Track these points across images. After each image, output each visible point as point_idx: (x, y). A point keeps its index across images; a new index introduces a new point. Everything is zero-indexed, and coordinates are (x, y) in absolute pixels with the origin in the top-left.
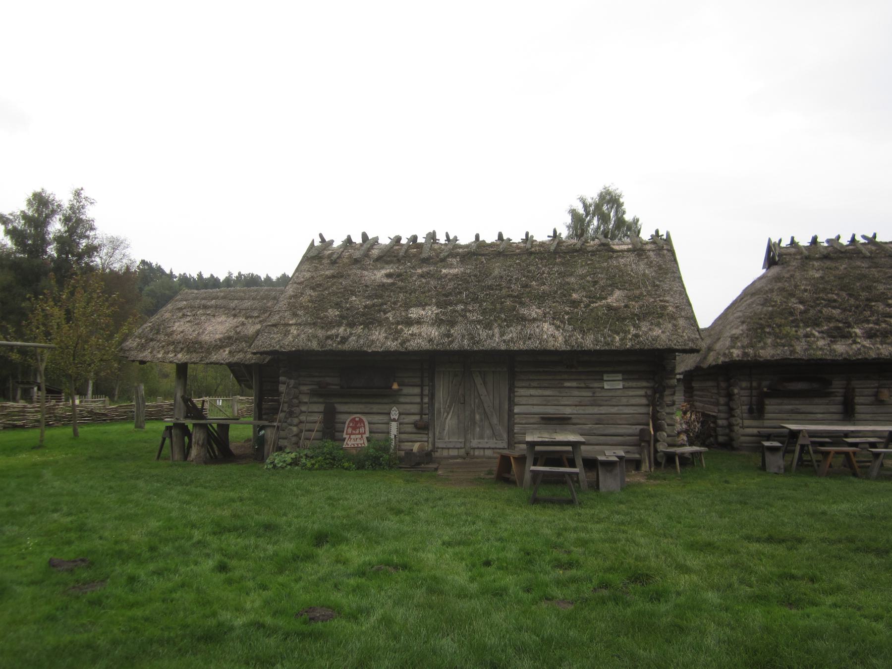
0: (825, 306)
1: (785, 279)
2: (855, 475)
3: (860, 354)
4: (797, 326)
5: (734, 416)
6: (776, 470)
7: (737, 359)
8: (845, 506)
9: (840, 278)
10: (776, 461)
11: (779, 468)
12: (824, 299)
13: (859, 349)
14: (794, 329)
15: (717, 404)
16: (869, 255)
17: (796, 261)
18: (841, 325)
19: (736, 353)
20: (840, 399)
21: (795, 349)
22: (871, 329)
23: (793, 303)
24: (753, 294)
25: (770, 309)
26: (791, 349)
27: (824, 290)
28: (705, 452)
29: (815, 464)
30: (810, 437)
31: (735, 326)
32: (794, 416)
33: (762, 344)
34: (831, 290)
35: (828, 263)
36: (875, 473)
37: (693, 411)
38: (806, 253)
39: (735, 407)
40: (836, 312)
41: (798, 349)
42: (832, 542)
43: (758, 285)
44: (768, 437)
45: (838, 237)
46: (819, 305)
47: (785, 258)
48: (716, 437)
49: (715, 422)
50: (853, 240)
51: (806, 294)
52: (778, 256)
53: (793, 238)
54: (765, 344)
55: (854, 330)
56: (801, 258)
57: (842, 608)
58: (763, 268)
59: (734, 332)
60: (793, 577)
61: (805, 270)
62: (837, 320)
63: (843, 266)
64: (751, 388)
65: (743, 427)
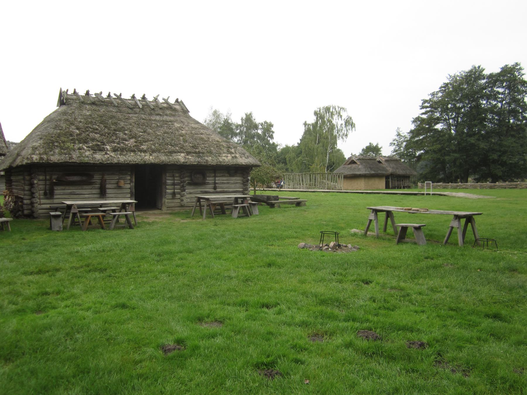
0: (91, 132)
1: (69, 114)
2: (103, 228)
3: (109, 160)
4: (74, 143)
5: (34, 198)
6: (58, 229)
7: (36, 161)
8: (90, 246)
9: (101, 117)
10: (58, 224)
11: (60, 227)
12: (91, 128)
13: (108, 158)
14: (72, 144)
15: (24, 190)
16: (117, 105)
17: (76, 104)
18: (99, 143)
19: (35, 158)
20: (98, 186)
21: (72, 156)
22: (116, 146)
23: (73, 128)
24: (49, 122)
25: (59, 131)
26: (70, 156)
27: (91, 123)
28: (11, 221)
29: (81, 224)
30: (78, 208)
31: (35, 141)
32: (72, 196)
33: (52, 153)
34: (95, 123)
35: (94, 107)
36: (113, 226)
37: (10, 195)
38: (82, 100)
39: (35, 192)
40: (97, 136)
41: (74, 156)
42: (77, 268)
43: (52, 117)
44: (56, 209)
45: (101, 93)
46: (87, 131)
47: (70, 101)
48: (23, 211)
49: (22, 202)
50: (156, 99)
51: (81, 124)
52: (66, 100)
53: (75, 90)
54: (54, 152)
55: (106, 147)
56: (80, 102)
57: (70, 307)
58: (57, 106)
59: (34, 144)
60: (47, 293)
61: (81, 110)
62: (97, 141)
63: (102, 110)
64: (46, 180)
65: (40, 204)
